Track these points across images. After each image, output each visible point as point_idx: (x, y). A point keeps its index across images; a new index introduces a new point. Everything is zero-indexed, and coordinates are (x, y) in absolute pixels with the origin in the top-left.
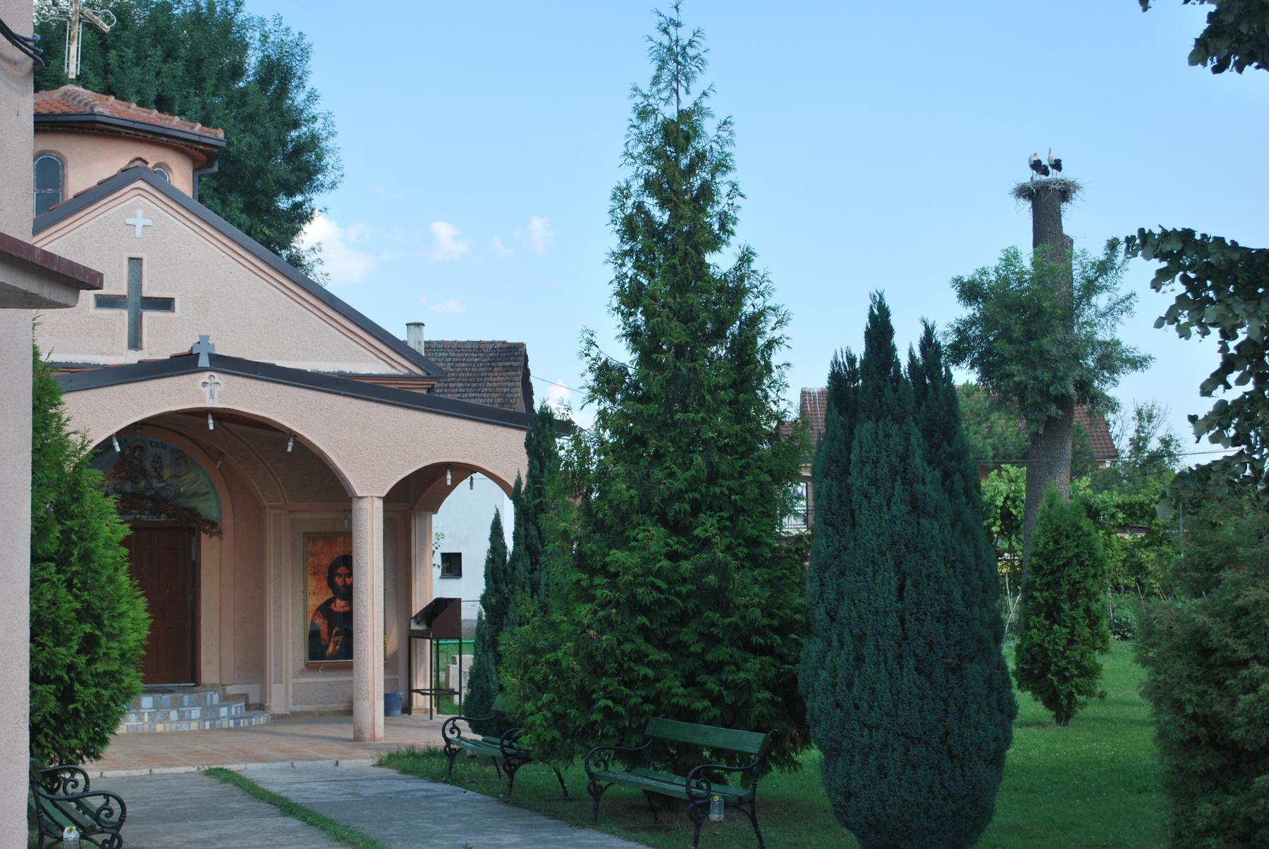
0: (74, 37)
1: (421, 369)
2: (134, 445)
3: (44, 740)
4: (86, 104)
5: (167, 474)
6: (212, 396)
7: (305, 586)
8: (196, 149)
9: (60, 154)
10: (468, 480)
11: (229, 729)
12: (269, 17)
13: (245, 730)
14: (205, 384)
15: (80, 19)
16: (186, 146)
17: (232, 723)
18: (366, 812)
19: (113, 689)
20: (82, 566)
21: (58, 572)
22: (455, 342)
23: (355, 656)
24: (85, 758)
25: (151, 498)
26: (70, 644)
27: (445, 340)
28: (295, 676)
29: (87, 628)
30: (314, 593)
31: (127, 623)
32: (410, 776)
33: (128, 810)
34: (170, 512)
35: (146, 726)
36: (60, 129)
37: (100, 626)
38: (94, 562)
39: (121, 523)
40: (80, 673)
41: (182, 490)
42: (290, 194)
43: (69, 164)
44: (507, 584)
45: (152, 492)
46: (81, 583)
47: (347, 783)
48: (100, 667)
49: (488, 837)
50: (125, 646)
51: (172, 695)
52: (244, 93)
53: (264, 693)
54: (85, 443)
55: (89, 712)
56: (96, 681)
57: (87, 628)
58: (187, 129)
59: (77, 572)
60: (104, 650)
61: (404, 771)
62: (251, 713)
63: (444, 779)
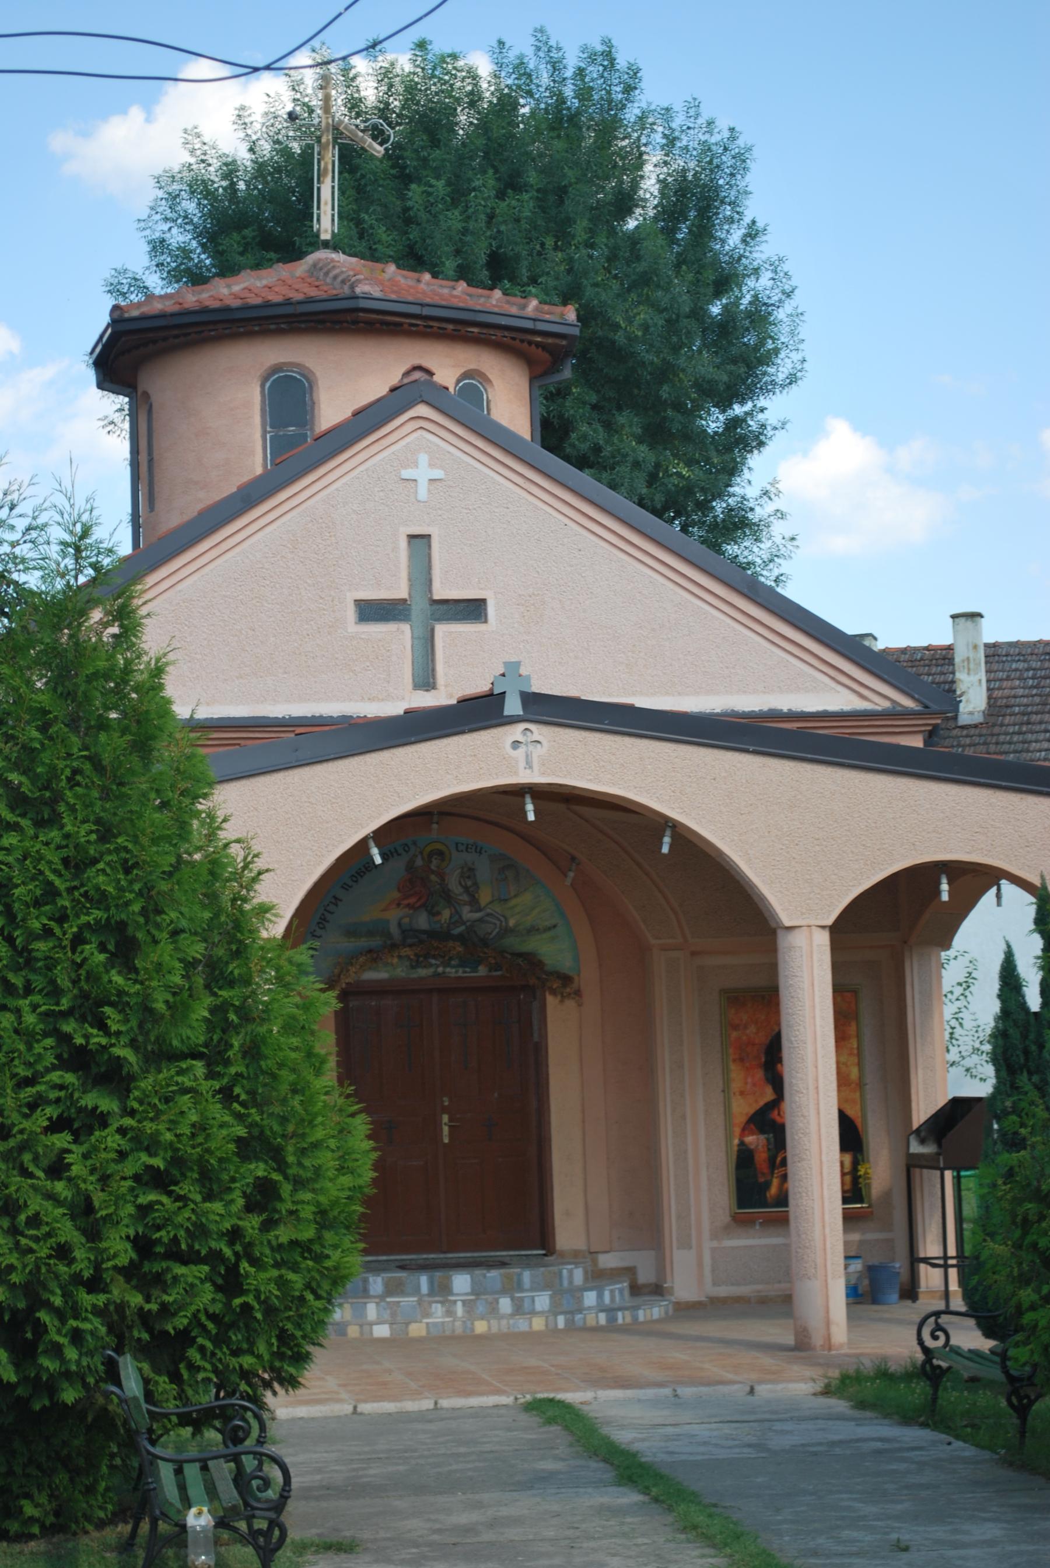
0: (326, 169)
1: (913, 697)
2: (428, 849)
3: (198, 1357)
4: (343, 282)
5: (485, 896)
6: (529, 765)
7: (727, 1082)
8: (530, 343)
9: (307, 368)
10: (994, 890)
11: (597, 1329)
12: (678, 106)
13: (624, 1330)
14: (516, 744)
15: (335, 139)
16: (513, 339)
17: (602, 1318)
18: (759, 1480)
19: (309, 1271)
20: (78, 1079)
21: (211, 1075)
22: (1040, 642)
23: (792, 1201)
24: (276, 1385)
25: (461, 938)
26: (228, 1197)
27: (912, 645)
28: (714, 1236)
29: (260, 1169)
30: (742, 1093)
31: (327, 1160)
32: (868, 1414)
33: (293, 1480)
34: (493, 961)
35: (458, 1324)
36: (303, 326)
37: (281, 1166)
38: (266, 1058)
39: (323, 990)
40: (250, 1244)
41: (512, 923)
42: (724, 405)
43: (320, 382)
44: (1030, 1073)
45: (463, 928)
46: (248, 1093)
47: (755, 1425)
48: (283, 1234)
49: (949, 1528)
50: (322, 1199)
51: (502, 1271)
52: (634, 239)
53: (661, 1267)
54: (249, 859)
55: (270, 1311)
56: (278, 1257)
57: (260, 1169)
58: (514, 310)
59: (237, 1074)
60: (290, 1206)
61: (861, 1405)
62: (639, 1300)
63: (922, 1419)
